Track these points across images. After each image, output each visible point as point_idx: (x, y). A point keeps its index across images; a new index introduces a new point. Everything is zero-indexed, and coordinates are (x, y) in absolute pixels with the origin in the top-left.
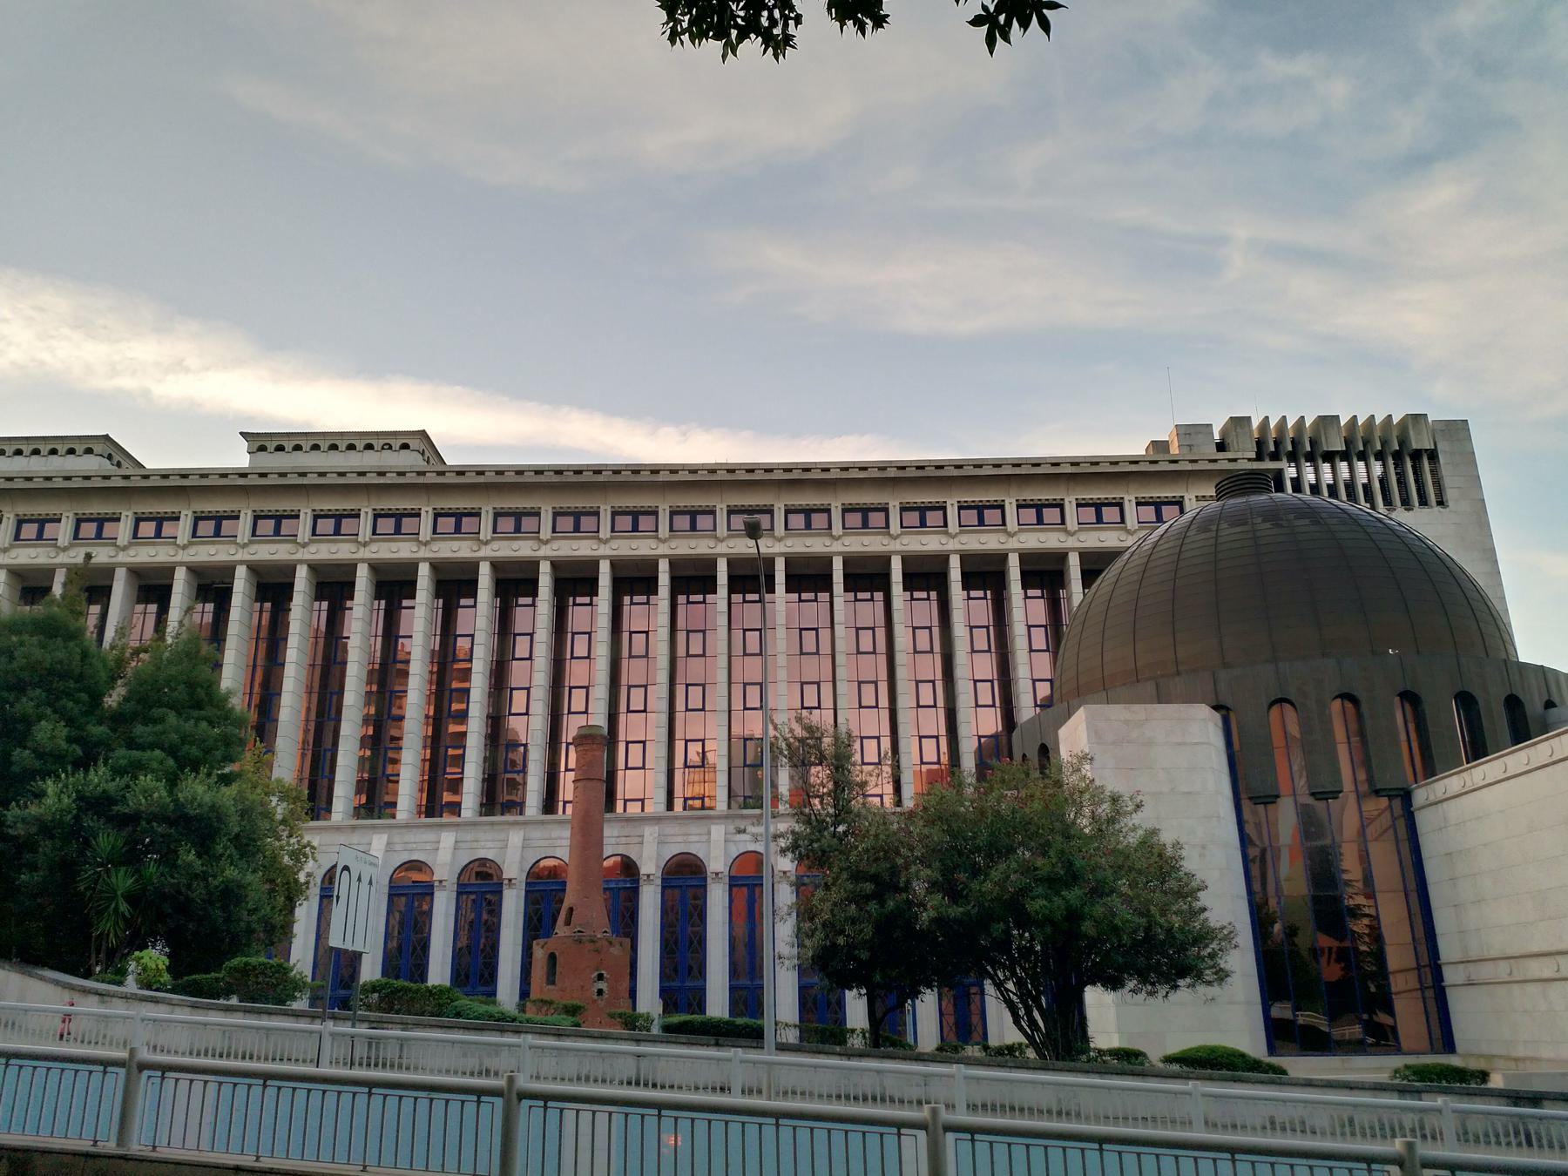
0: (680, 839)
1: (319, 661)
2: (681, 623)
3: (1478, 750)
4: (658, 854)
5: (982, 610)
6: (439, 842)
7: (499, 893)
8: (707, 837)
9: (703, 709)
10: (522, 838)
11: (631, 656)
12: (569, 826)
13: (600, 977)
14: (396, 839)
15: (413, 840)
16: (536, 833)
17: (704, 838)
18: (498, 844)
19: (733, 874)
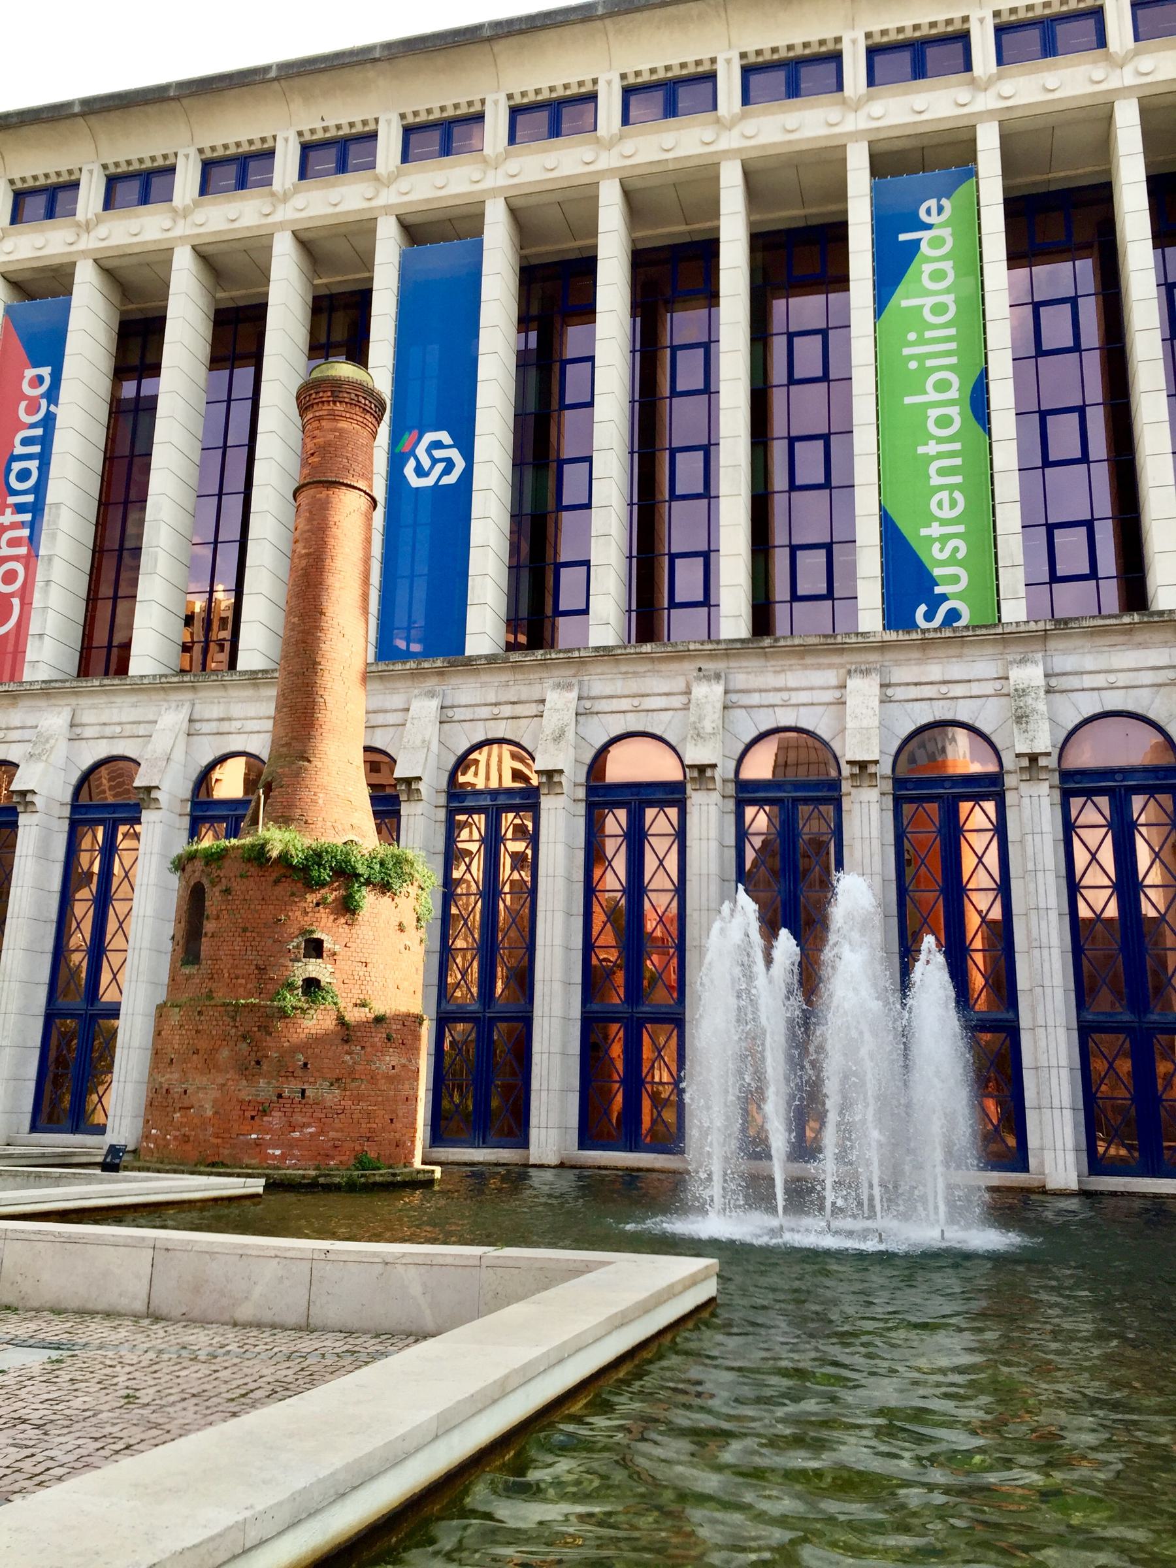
0: (625, 704)
3: (106, 674)
4: (882, 725)
8: (683, 699)
10: (66, 725)
11: (792, 381)
14: (87, 717)
15: (115, 719)
19: (902, 773)
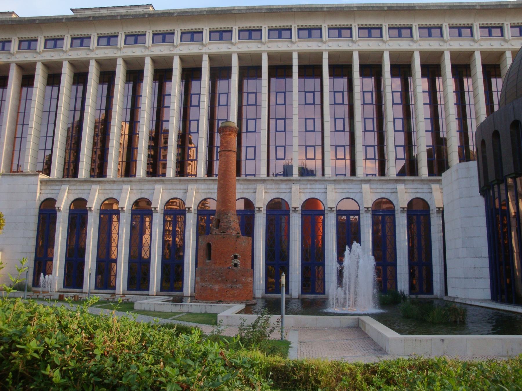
1: (156, 106)
2: (273, 89)
5: (370, 83)
6: (154, 189)
7: (87, 214)
9: (285, 131)
11: (248, 105)
12: (217, 182)
13: (236, 257)
16: (202, 186)
17: (288, 191)
18: (184, 191)
